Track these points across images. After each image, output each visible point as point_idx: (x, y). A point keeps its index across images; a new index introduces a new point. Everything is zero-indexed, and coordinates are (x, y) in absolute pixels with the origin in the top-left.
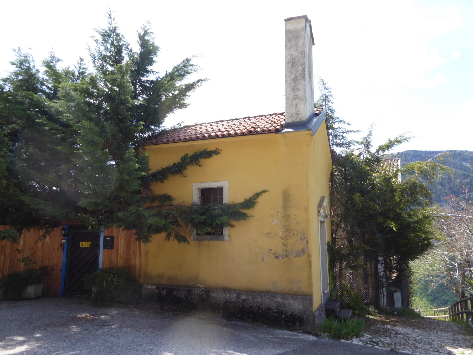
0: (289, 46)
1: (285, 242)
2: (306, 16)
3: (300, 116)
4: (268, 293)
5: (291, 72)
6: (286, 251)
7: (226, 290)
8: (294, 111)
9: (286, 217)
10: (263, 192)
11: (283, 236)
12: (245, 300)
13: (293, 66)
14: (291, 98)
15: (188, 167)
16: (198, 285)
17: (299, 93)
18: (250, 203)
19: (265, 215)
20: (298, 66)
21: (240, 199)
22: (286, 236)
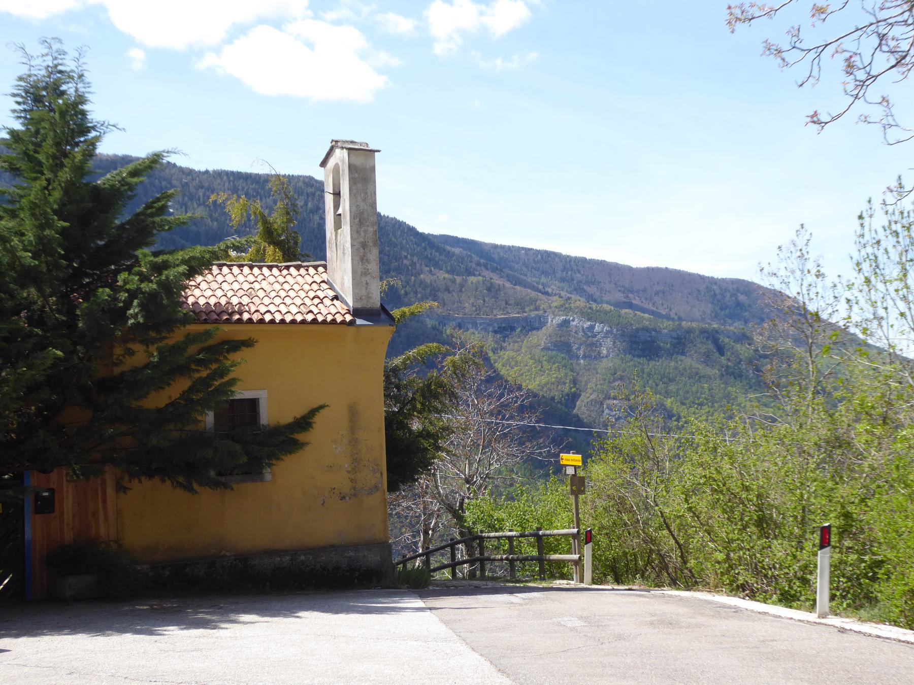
0: (355, 191)
1: (353, 477)
2: (103, 9)
3: (372, 301)
4: (333, 547)
5: (358, 232)
6: (354, 488)
7: (270, 553)
8: (364, 293)
9: (354, 442)
10: (322, 407)
11: (349, 469)
12: (303, 562)
13: (361, 223)
14: (359, 273)
15: (242, 393)
16: (223, 553)
17: (370, 267)
18: (304, 423)
19: (325, 444)
20: (368, 226)
21: (287, 418)
22: (353, 469)
